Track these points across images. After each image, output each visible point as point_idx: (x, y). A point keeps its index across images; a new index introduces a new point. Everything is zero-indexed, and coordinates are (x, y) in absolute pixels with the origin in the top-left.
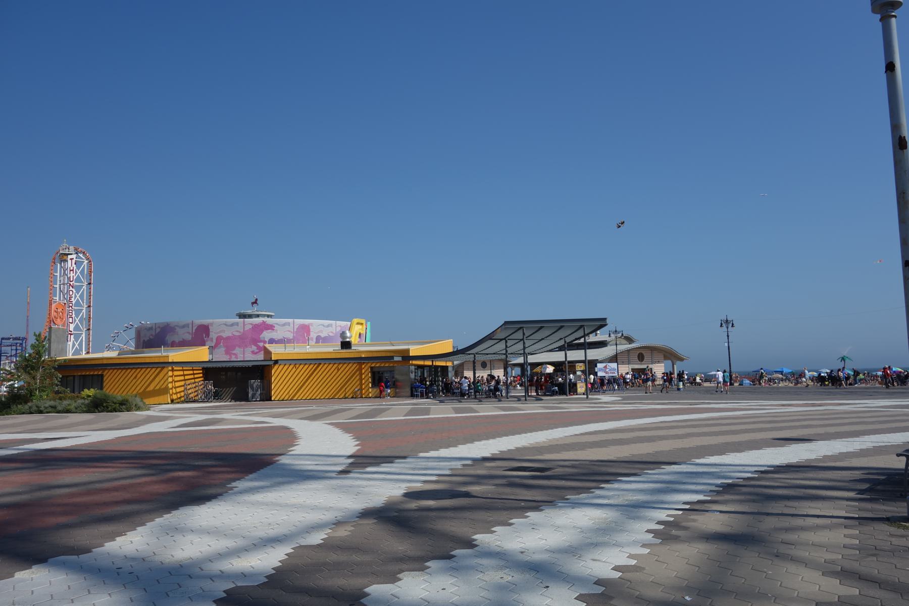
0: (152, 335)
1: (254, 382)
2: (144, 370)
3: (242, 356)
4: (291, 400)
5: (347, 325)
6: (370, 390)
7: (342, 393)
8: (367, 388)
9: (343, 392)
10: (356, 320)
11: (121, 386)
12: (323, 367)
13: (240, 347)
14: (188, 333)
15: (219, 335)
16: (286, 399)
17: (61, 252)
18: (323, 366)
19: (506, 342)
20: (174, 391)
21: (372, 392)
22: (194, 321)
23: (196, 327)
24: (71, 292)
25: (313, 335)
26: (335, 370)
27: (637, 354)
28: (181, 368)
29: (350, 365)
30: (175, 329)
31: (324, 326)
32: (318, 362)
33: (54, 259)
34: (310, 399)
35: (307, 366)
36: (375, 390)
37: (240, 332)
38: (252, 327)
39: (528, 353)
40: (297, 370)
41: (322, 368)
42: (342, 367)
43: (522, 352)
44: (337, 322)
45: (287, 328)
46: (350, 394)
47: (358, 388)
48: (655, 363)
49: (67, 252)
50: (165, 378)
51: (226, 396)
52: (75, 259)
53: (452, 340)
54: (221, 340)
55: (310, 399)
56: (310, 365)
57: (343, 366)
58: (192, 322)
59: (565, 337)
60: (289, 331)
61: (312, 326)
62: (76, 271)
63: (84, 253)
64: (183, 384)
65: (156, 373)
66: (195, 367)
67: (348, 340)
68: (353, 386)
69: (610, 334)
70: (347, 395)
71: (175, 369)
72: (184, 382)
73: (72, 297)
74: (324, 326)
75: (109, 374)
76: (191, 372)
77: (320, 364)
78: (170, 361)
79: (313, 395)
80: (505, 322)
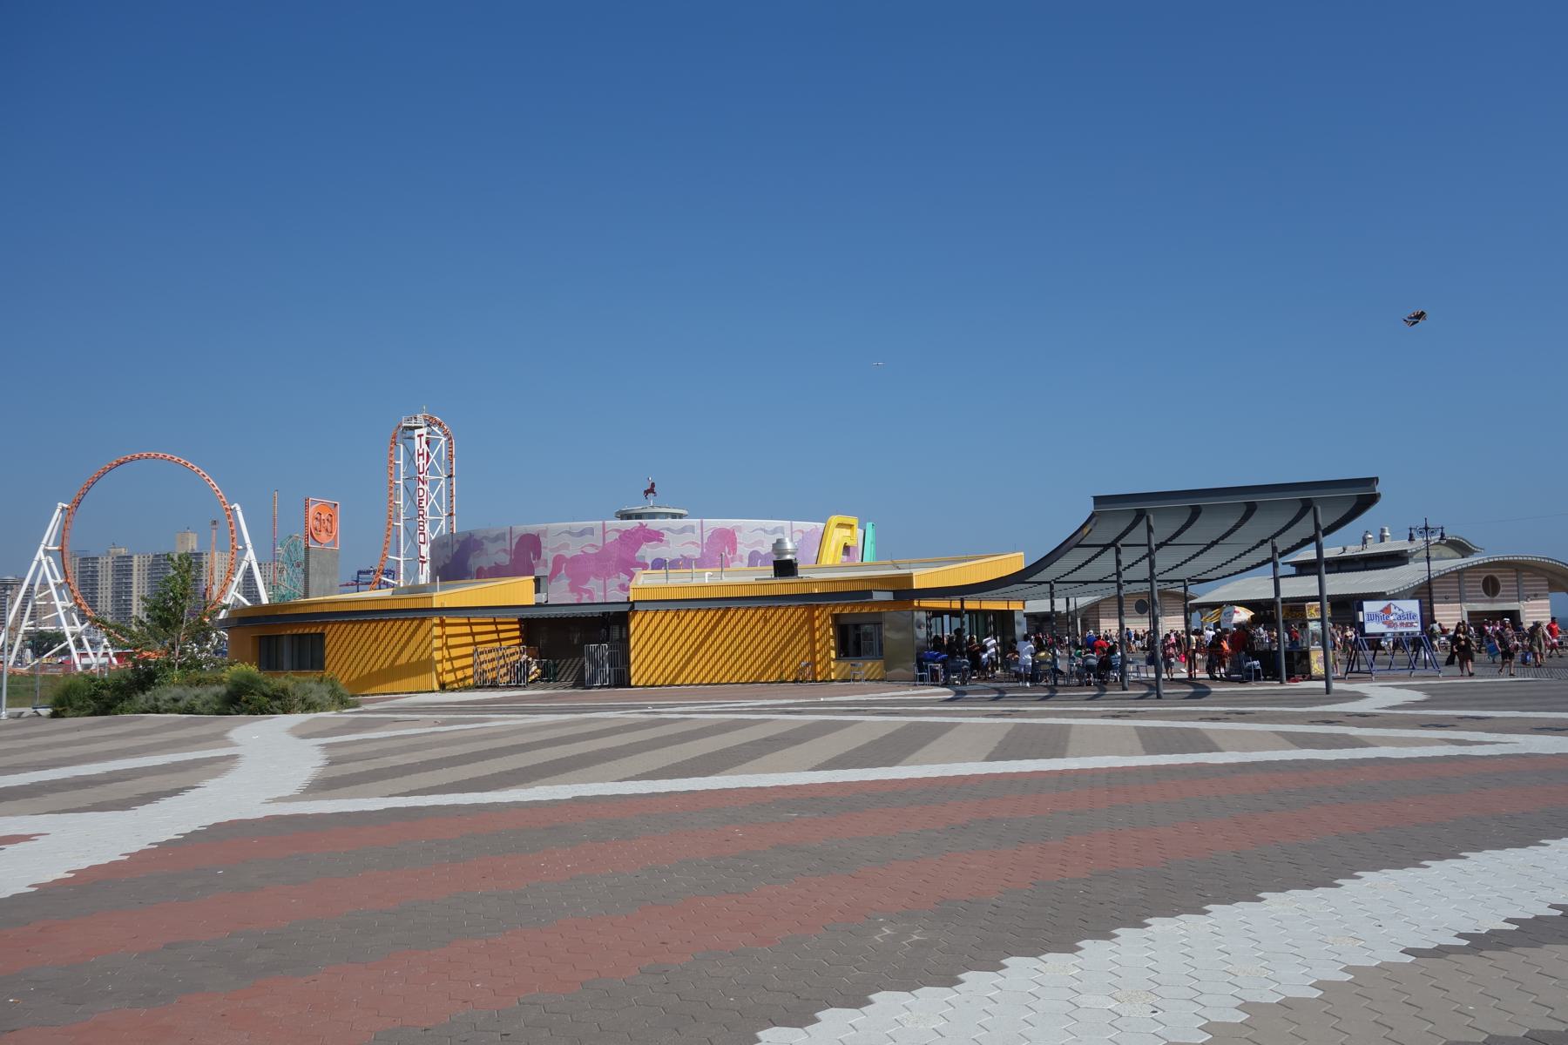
0: (448, 557)
1: (596, 650)
2: (390, 624)
3: (602, 594)
4: (669, 685)
5: (817, 529)
6: (833, 665)
7: (774, 671)
8: (825, 661)
9: (777, 669)
10: (835, 519)
11: (352, 656)
12: (736, 617)
13: (597, 576)
14: (505, 550)
16: (659, 683)
17: (404, 425)
18: (734, 614)
19: (1118, 552)
20: (448, 666)
21: (836, 668)
22: (513, 527)
24: (421, 491)
25: (743, 550)
26: (758, 621)
27: (1482, 580)
28: (466, 621)
29: (790, 611)
30: (483, 545)
31: (765, 531)
32: (724, 604)
33: (394, 437)
34: (699, 684)
35: (701, 614)
36: (843, 664)
37: (597, 547)
38: (620, 537)
39: (1190, 580)
40: (681, 621)
41: (732, 617)
42: (773, 615)
43: (1114, 578)
45: (689, 536)
46: (791, 673)
47: (808, 659)
48: (1527, 598)
49: (413, 425)
50: (428, 640)
51: (568, 673)
52: (425, 436)
53: (1022, 554)
54: (563, 563)
55: (699, 684)
56: (707, 612)
57: (775, 612)
58: (511, 528)
59: (1273, 537)
60: (693, 543)
61: (740, 532)
62: (428, 453)
63: (440, 424)
64: (471, 652)
65: (411, 629)
66: (498, 617)
67: (788, 557)
68: (796, 657)
69: (1411, 535)
70: (784, 676)
71: (447, 621)
72: (473, 647)
74: (765, 531)
75: (333, 632)
76: (492, 628)
77: (728, 609)
78: (434, 606)
79: (716, 674)
80: (1303, 539)
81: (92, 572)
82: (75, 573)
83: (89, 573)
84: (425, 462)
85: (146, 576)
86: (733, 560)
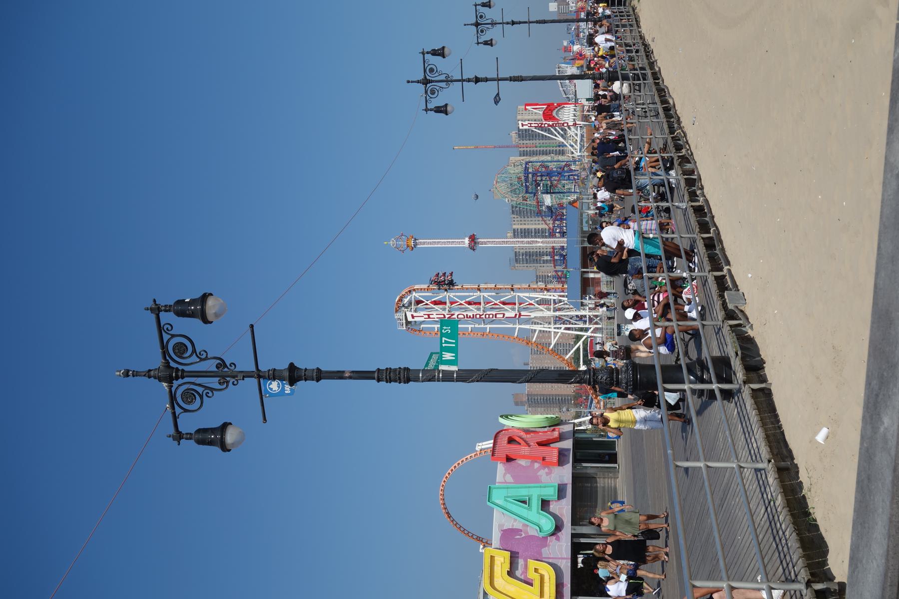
24: (460, 316)
38: (509, 473)
44: (497, 481)
61: (503, 525)
73: (467, 315)
81: (526, 255)
82: (527, 267)
83: (528, 257)
84: (434, 313)
85: (530, 219)
86: (526, 532)
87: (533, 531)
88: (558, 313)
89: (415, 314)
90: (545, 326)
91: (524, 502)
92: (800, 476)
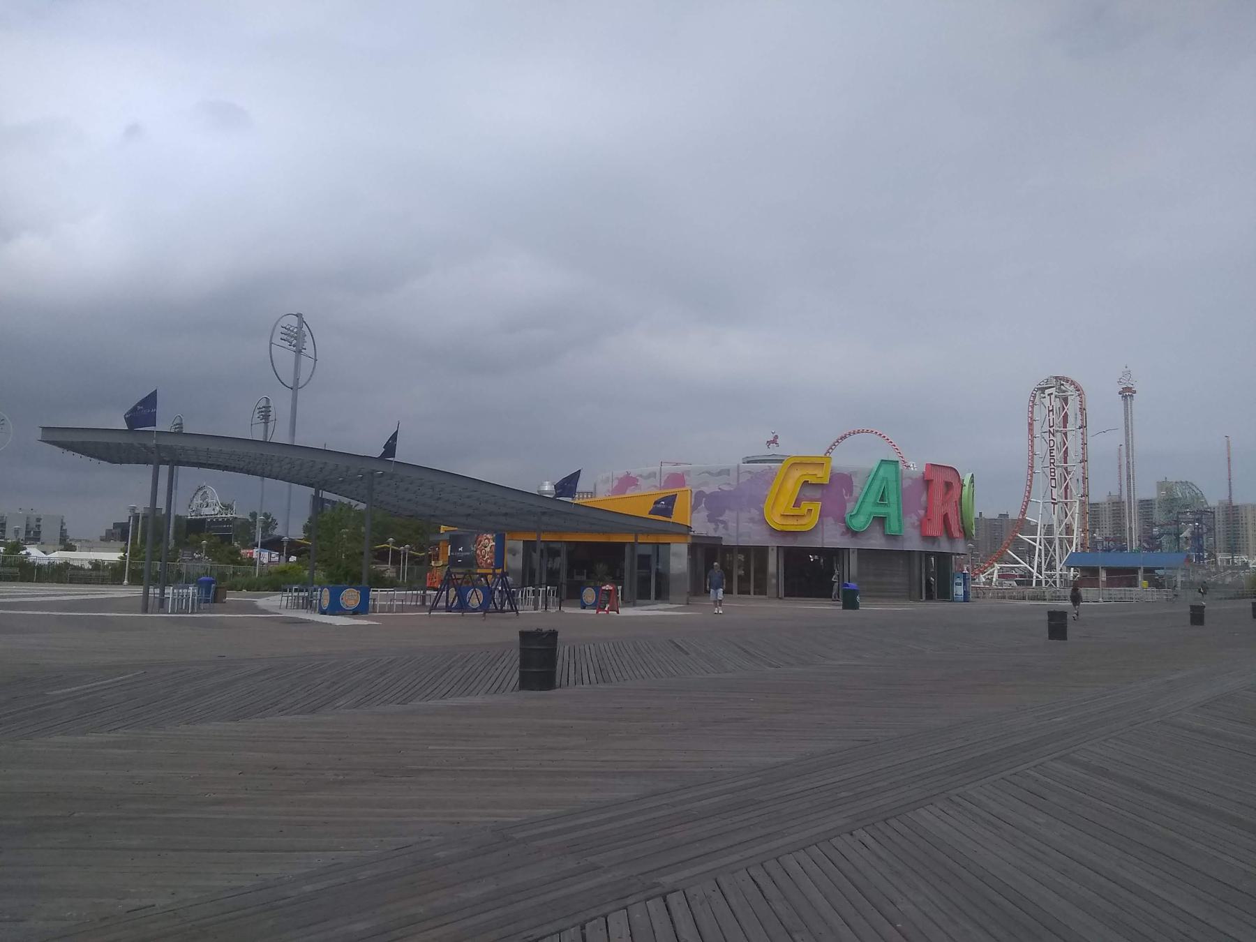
15: (700, 490)
23: (666, 478)
87: (851, 508)
88: (1057, 542)
89: (1053, 396)
90: (1042, 529)
91: (882, 499)
92: (534, 629)
